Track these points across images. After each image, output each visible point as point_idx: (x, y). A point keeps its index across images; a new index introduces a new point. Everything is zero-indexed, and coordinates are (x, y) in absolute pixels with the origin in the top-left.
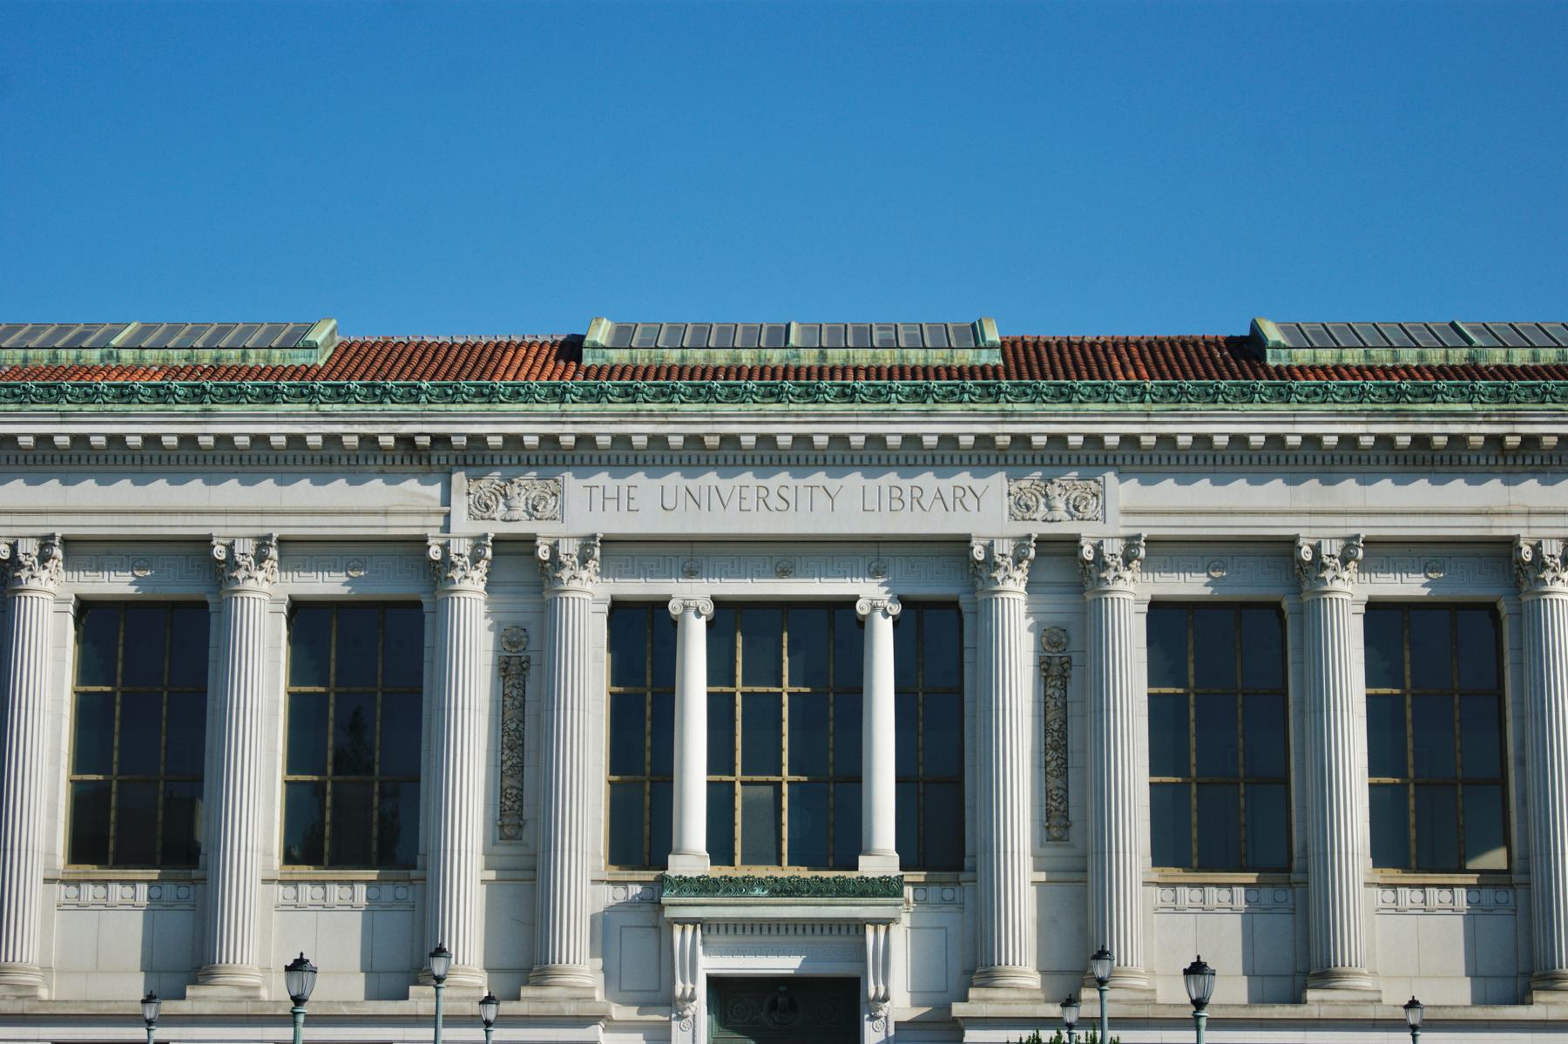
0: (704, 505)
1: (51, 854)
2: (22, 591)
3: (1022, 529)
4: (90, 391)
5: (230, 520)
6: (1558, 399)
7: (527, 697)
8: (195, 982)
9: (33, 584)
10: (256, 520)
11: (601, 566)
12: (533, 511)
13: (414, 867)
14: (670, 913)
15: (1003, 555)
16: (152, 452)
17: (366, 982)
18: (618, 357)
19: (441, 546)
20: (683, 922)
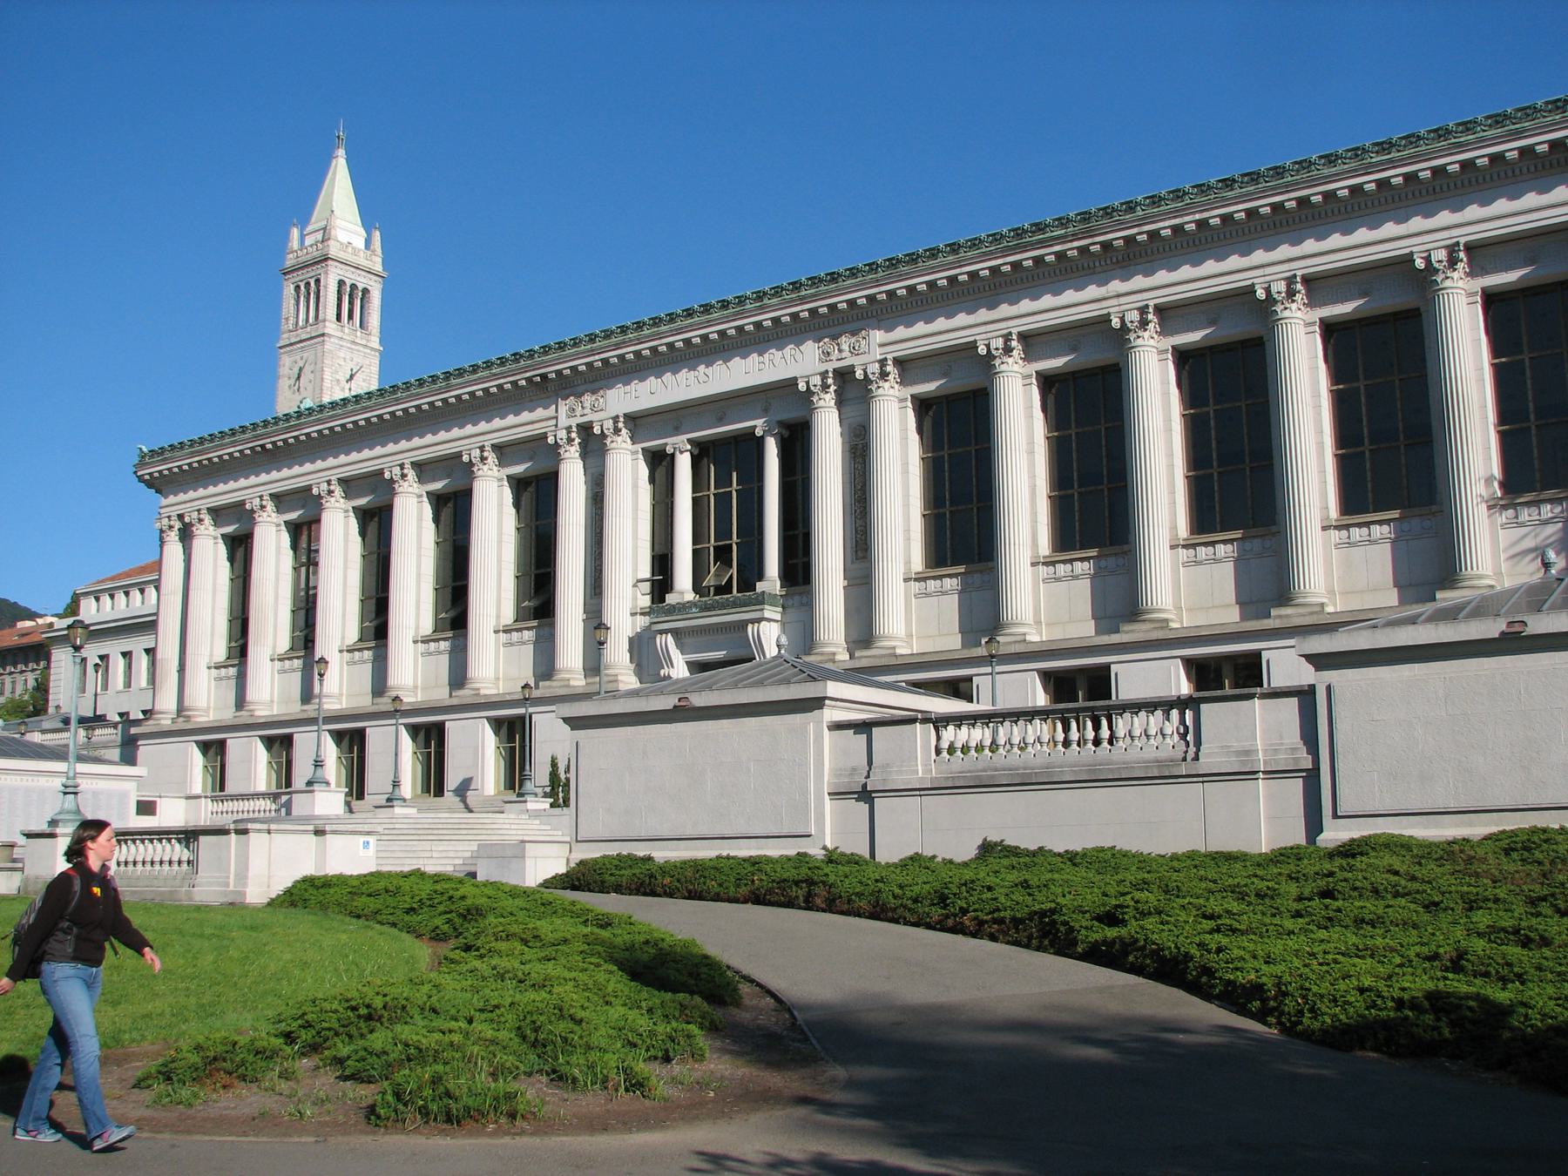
0: (669, 388)
1: (1174, 528)
2: (1133, 347)
3: (823, 367)
4: (1020, 232)
5: (389, 459)
6: (1401, 148)
8: (1443, 588)
9: (880, 391)
10: (1445, 234)
11: (1470, 266)
12: (854, 351)
15: (815, 386)
16: (1305, 212)
17: (1096, 626)
19: (1265, 289)
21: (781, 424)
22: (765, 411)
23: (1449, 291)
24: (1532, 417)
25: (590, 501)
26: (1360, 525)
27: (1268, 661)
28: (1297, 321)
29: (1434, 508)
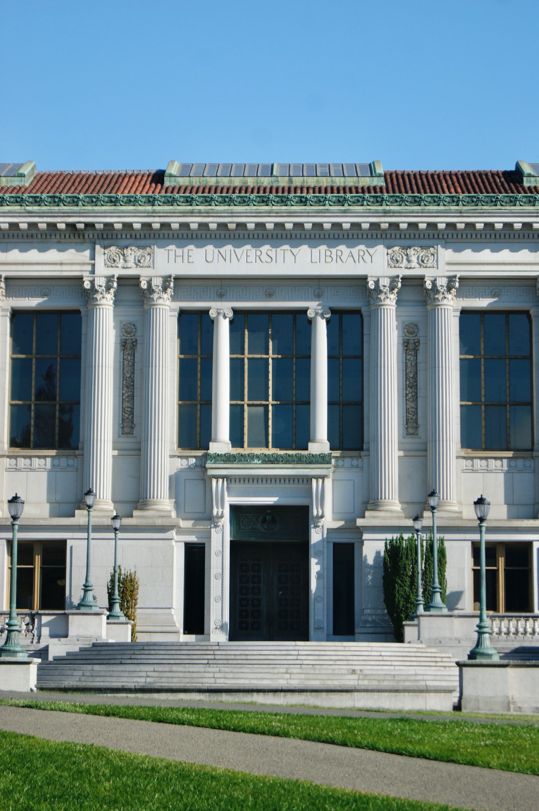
0: (228, 259)
3: (394, 272)
7: (136, 360)
11: (174, 292)
12: (138, 263)
13: (77, 449)
14: (211, 472)
18: (183, 182)
19: (375, 282)
20: (217, 477)
21: (333, 311)
22: (318, 296)
23: (445, 307)
24: (33, 398)
25: (119, 346)
26: (25, 457)
27: (71, 547)
28: (449, 307)
29: (77, 452)
